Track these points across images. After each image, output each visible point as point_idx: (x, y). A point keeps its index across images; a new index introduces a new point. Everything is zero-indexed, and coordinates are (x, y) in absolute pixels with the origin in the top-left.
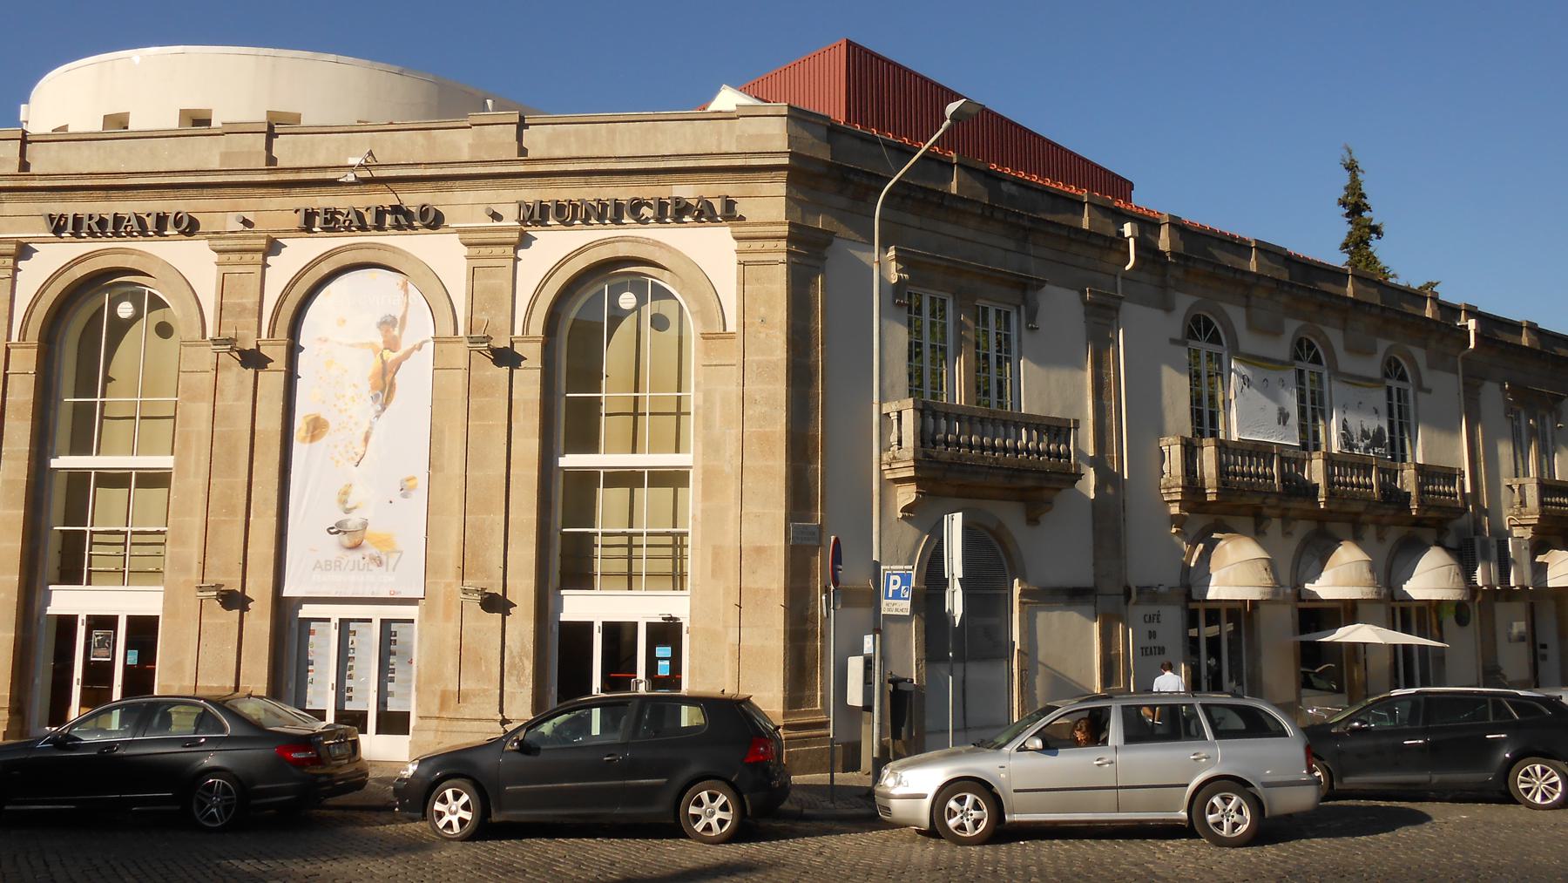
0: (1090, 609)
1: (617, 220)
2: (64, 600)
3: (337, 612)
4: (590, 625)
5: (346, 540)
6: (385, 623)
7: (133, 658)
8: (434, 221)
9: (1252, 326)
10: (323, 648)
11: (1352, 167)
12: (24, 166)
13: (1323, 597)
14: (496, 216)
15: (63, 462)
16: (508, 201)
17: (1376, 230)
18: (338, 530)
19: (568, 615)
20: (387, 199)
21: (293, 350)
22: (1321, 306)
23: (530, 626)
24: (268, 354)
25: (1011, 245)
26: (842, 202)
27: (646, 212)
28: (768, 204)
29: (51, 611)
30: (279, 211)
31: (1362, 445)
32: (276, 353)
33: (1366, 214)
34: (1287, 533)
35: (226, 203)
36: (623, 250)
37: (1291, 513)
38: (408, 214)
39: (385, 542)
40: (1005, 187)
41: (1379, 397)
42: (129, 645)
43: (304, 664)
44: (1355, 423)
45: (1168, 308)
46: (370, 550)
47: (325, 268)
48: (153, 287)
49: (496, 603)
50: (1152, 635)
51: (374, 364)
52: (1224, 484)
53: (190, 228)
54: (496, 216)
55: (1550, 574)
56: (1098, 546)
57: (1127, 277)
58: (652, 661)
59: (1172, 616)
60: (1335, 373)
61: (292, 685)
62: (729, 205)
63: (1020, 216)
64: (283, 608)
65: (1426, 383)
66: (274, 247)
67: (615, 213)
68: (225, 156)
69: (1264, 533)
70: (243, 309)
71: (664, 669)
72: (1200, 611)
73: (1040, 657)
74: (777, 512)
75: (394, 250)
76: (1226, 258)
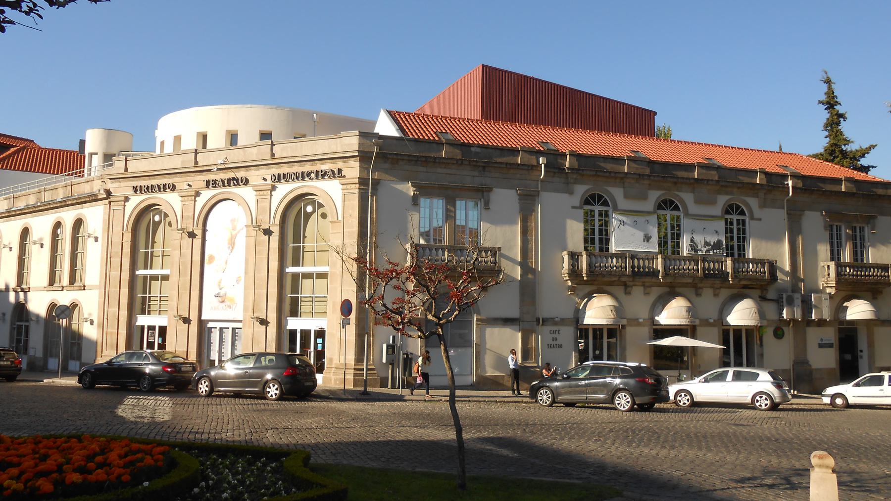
0: (517, 327)
1: (303, 179)
2: (143, 320)
3: (231, 325)
4: (310, 331)
5: (220, 299)
6: (234, 329)
7: (160, 341)
8: (246, 182)
9: (626, 196)
10: (215, 337)
11: (828, 82)
12: (126, 169)
13: (662, 323)
14: (265, 179)
15: (140, 272)
16: (268, 173)
17: (841, 116)
18: (217, 296)
19: (289, 327)
20: (230, 175)
21: (204, 231)
22: (675, 183)
23: (274, 330)
24: (197, 233)
25: (476, 173)
26: (387, 166)
27: (313, 175)
28: (353, 170)
29: (137, 324)
30: (199, 181)
31: (704, 249)
32: (198, 232)
33: (837, 107)
34: (716, 295)
35: (183, 179)
36: (305, 191)
37: (647, 284)
38: (237, 180)
39: (232, 300)
40: (473, 149)
41: (721, 225)
42: (159, 336)
43: (210, 344)
44: (700, 240)
45: (571, 193)
46: (227, 303)
47: (213, 201)
48: (164, 209)
49: (264, 322)
50: (555, 339)
51: (229, 236)
52: (591, 272)
53: (173, 188)
54: (265, 179)
55: (848, 312)
56: (522, 301)
57: (542, 181)
58: (316, 344)
59: (567, 333)
60: (687, 215)
61: (206, 351)
62: (340, 171)
63: (477, 162)
64: (202, 323)
65: (756, 216)
66: (198, 194)
67: (303, 176)
68: (183, 162)
69: (630, 293)
70: (188, 217)
71: (320, 348)
72: (583, 332)
73: (488, 346)
74: (354, 287)
75: (230, 193)
76: (609, 166)
